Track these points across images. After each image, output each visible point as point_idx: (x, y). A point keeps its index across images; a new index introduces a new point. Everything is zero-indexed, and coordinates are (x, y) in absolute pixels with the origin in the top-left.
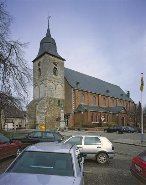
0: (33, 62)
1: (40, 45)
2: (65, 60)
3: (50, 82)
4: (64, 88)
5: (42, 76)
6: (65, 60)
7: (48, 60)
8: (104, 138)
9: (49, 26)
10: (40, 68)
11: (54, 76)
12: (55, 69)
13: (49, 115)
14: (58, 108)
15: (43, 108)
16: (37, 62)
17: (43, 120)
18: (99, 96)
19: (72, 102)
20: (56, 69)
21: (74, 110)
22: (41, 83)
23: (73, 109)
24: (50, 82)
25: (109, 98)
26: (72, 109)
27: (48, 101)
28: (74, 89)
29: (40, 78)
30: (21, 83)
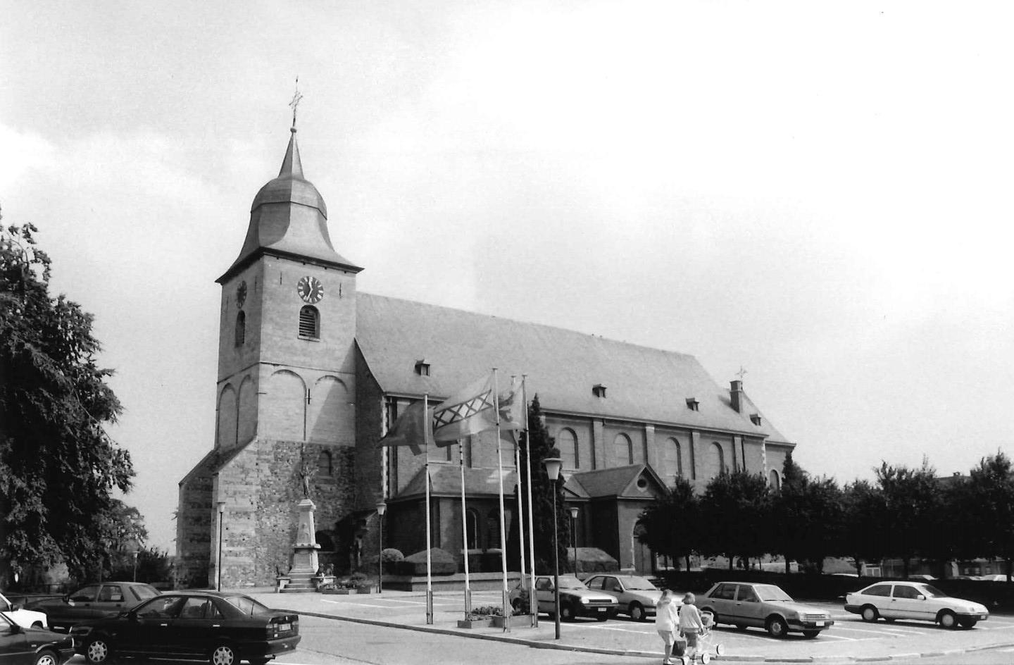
0: (223, 280)
1: (251, 212)
2: (358, 270)
3: (279, 372)
4: (352, 395)
5: (249, 345)
6: (358, 270)
7: (277, 281)
8: (206, 455)
9: (293, 131)
10: (244, 308)
11: (299, 344)
12: (311, 312)
13: (273, 518)
14: (317, 488)
15: (243, 488)
16: (235, 284)
17: (240, 544)
18: (644, 431)
19: (381, 458)
20: (315, 310)
21: (388, 493)
22: (243, 375)
23: (385, 488)
24: (279, 372)
25: (598, 426)
26: (381, 489)
27: (269, 457)
28: (388, 398)
29: (241, 355)
30: (297, 98)
